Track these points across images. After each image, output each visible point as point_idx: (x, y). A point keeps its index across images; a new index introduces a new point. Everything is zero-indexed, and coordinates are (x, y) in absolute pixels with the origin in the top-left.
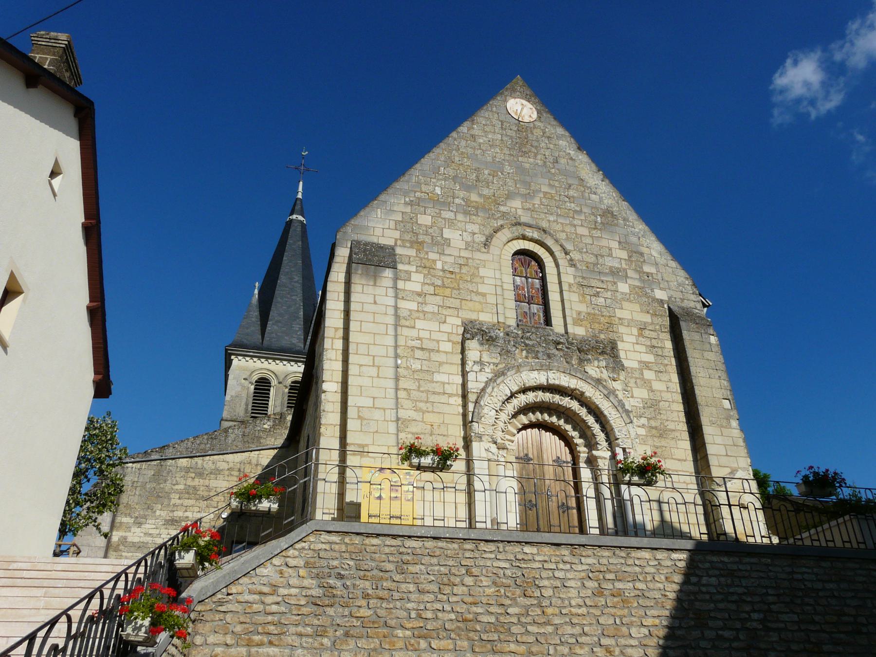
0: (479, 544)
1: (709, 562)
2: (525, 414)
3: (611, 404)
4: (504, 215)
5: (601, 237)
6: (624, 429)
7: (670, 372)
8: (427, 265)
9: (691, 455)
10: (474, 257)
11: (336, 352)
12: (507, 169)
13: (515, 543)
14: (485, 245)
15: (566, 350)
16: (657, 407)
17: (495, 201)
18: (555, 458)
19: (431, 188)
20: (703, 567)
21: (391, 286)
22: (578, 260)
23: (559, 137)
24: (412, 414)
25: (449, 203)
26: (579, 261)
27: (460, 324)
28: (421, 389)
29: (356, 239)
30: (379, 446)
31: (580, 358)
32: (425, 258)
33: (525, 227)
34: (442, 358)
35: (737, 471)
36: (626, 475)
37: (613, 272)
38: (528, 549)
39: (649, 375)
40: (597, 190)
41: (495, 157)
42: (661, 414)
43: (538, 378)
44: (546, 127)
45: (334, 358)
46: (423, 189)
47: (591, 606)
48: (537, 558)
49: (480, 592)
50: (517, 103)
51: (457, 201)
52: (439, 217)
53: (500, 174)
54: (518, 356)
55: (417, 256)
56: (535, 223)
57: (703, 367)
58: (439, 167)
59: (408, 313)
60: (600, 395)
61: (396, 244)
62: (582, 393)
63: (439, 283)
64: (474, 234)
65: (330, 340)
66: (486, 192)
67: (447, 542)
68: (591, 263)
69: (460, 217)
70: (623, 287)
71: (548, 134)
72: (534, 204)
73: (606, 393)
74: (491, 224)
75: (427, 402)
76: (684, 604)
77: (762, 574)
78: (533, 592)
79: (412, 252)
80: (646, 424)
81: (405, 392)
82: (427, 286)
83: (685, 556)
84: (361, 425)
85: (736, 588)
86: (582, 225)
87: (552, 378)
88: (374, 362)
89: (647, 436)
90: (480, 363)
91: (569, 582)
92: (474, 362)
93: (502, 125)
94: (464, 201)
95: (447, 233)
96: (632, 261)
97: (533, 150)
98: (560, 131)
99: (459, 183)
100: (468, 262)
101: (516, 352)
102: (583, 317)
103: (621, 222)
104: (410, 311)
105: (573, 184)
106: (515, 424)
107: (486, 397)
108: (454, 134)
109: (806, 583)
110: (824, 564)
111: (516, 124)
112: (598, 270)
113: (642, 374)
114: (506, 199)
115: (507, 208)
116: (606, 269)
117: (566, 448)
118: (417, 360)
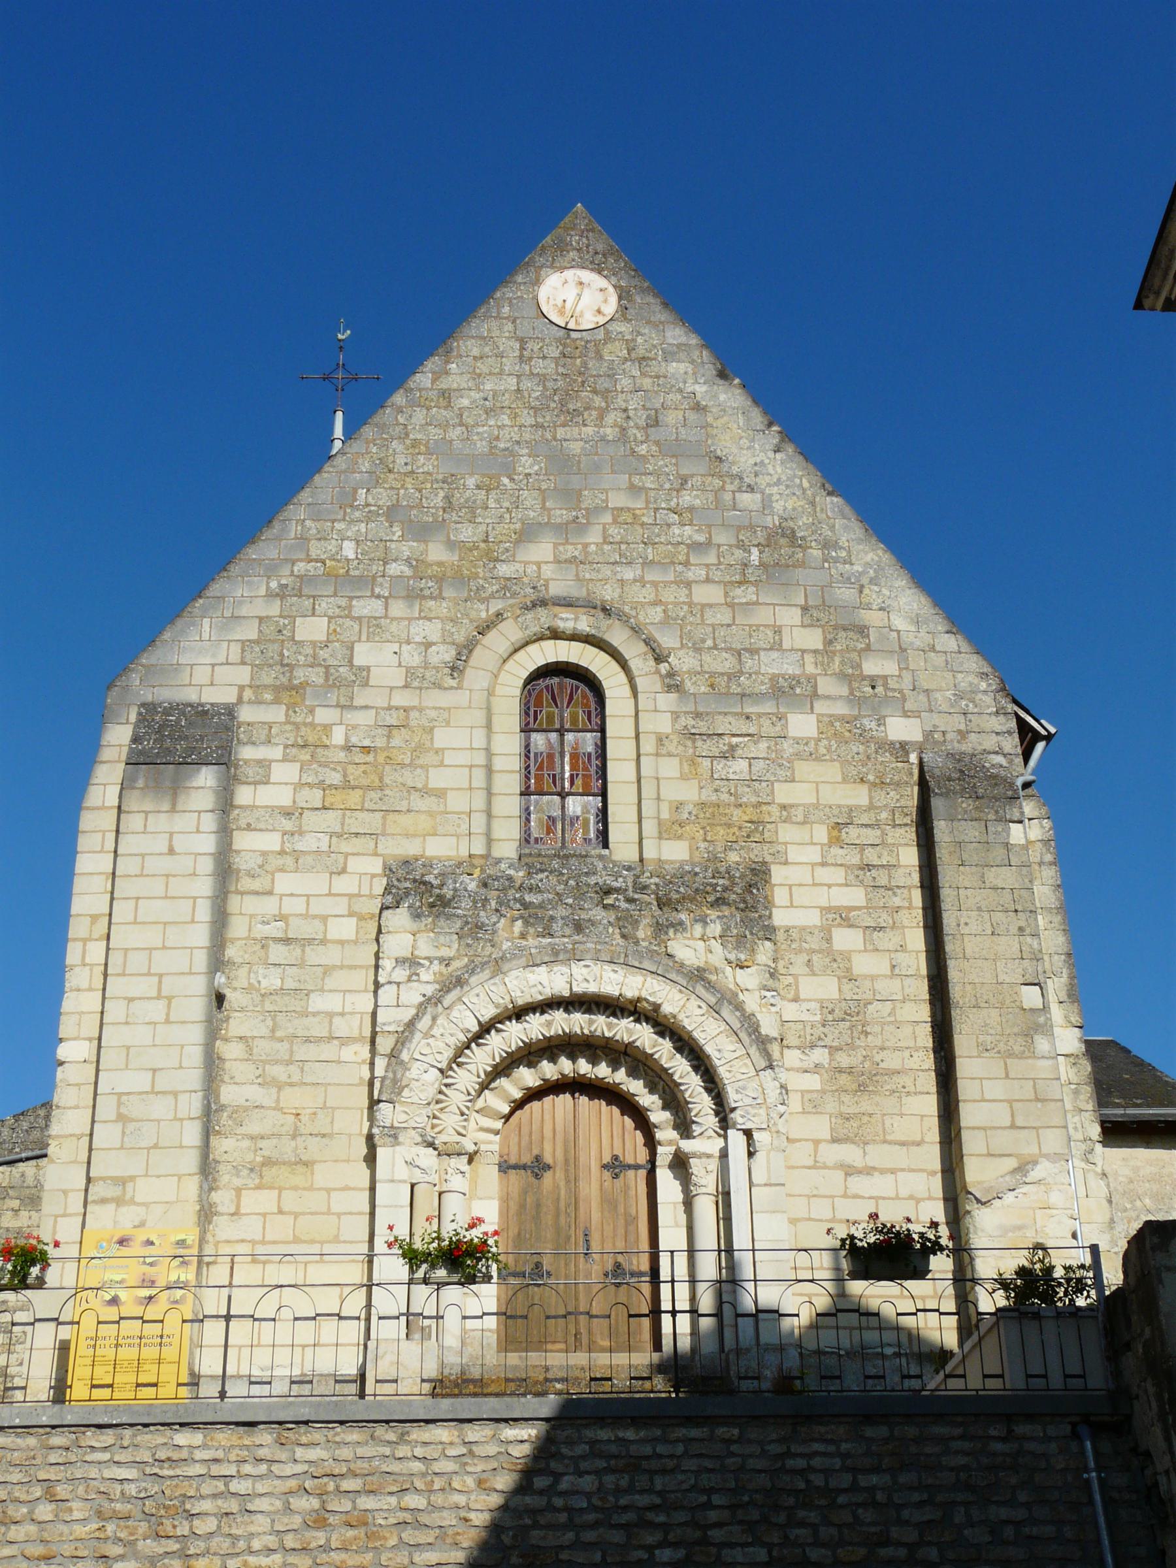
0: (84, 1433)
1: (586, 1443)
2: (531, 1065)
3: (723, 1026)
4: (507, 586)
5: (757, 603)
6: (754, 1084)
7: (904, 927)
8: (311, 740)
9: (936, 1130)
10: (424, 704)
11: (91, 970)
12: (526, 464)
13: (159, 1427)
14: (453, 668)
15: (624, 905)
16: (860, 1018)
17: (488, 552)
18: (607, 1159)
19: (332, 546)
20: (570, 1454)
21: (210, 807)
22: (689, 672)
23: (669, 356)
24: (255, 1094)
25: (374, 578)
26: (693, 673)
27: (379, 870)
28: (279, 1034)
29: (149, 698)
30: (158, 1177)
31: (657, 923)
32: (305, 724)
33: (557, 609)
34: (331, 955)
35: (1035, 1163)
36: (419, 1267)
37: (780, 689)
38: (183, 1438)
39: (846, 939)
40: (759, 480)
41: (497, 438)
42: (867, 1034)
43: (546, 983)
44: (639, 334)
45: (86, 985)
46: (314, 554)
47: (294, 1550)
48: (199, 1455)
49: (61, 1535)
50: (566, 282)
51: (394, 569)
52: (347, 617)
53: (505, 480)
54: (502, 934)
55: (288, 722)
56: (584, 593)
57: (979, 909)
58: (355, 491)
59: (260, 861)
60: (700, 1007)
61: (240, 700)
62: (657, 1007)
63: (335, 778)
64: (428, 645)
65: (80, 944)
66: (467, 533)
67: (17, 1435)
68: (722, 674)
69: (398, 608)
70: (802, 725)
71: (641, 352)
72: (586, 546)
73: (712, 1000)
74: (473, 614)
75: (289, 1062)
76: (503, 1537)
77: (708, 1464)
78: (174, 1527)
79: (276, 714)
80: (826, 1063)
81: (241, 1046)
82: (306, 791)
83: (533, 1432)
84: (124, 1133)
85: (637, 1497)
86: (708, 580)
87: (580, 978)
88: (159, 990)
89: (823, 1092)
90: (411, 962)
91: (257, 1501)
92: (397, 960)
93: (522, 349)
94: (411, 566)
95: (363, 655)
96: (834, 653)
97: (598, 401)
98: (677, 334)
99: (402, 523)
100: (407, 717)
101: (500, 925)
102: (686, 815)
103: (816, 553)
104: (264, 854)
105: (692, 476)
106: (505, 1091)
107: (415, 1041)
108: (399, 398)
109: (812, 1477)
110: (869, 1432)
111: (559, 340)
112: (739, 690)
113: (829, 940)
114: (518, 542)
115: (518, 566)
116: (762, 683)
117: (638, 1133)
118: (272, 968)
